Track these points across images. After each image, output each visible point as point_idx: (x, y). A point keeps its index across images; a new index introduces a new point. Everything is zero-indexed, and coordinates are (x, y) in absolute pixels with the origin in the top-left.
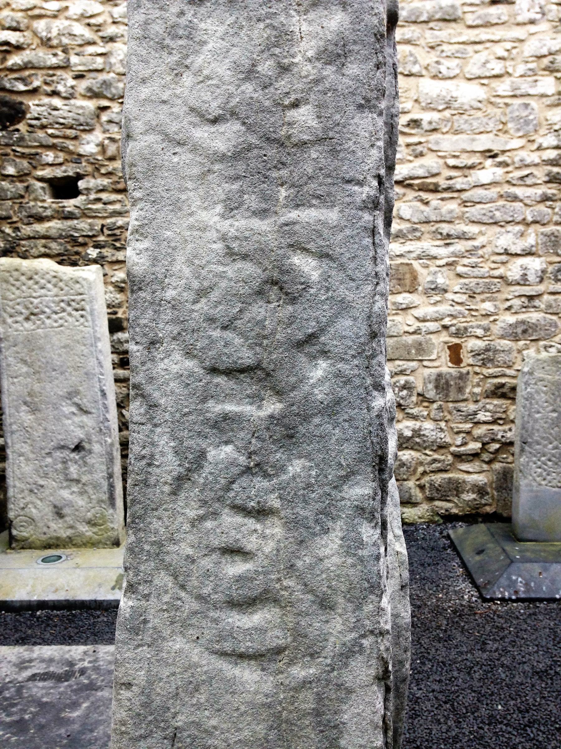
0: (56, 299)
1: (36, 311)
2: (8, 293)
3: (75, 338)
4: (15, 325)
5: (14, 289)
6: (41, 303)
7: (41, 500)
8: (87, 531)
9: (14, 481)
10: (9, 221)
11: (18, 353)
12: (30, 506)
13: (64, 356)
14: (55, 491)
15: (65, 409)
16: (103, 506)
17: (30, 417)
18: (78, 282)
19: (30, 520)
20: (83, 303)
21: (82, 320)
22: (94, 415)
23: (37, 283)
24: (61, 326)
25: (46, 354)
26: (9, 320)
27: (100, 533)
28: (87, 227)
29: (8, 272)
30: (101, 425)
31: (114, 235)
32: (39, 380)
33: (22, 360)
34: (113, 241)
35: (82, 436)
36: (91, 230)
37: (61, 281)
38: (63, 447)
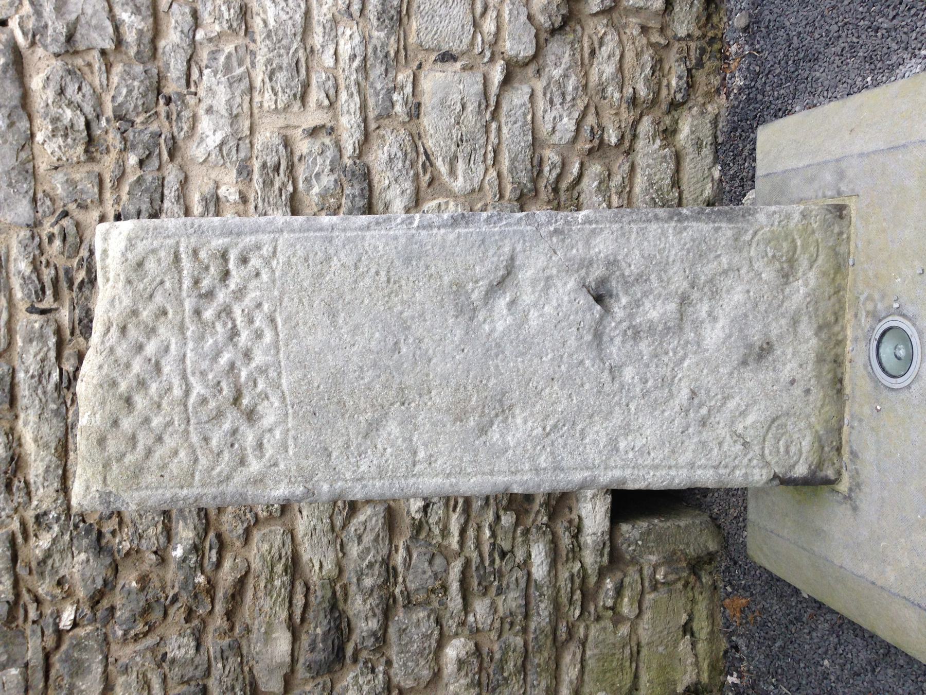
0: (191, 329)
1: (227, 391)
2: (174, 467)
3: (306, 284)
4: (269, 452)
5: (160, 452)
6: (203, 374)
7: (726, 399)
8: (806, 285)
9: (676, 466)
10: (20, 540)
11: (347, 446)
12: (740, 428)
13: (357, 318)
14: (707, 361)
15: (500, 326)
16: (748, 237)
17: (519, 421)
18: (140, 264)
19: (774, 428)
20: (203, 255)
21: (255, 262)
22: (519, 247)
23: (142, 384)
24: (272, 320)
25: (352, 367)
26: (255, 466)
27: (812, 249)
28: (34, 348)
29: (106, 466)
30: (544, 231)
31: (55, 282)
32: (425, 390)
33: (366, 436)
34: (71, 288)
35: (571, 284)
36: (42, 337)
37: (135, 313)
38: (598, 335)
